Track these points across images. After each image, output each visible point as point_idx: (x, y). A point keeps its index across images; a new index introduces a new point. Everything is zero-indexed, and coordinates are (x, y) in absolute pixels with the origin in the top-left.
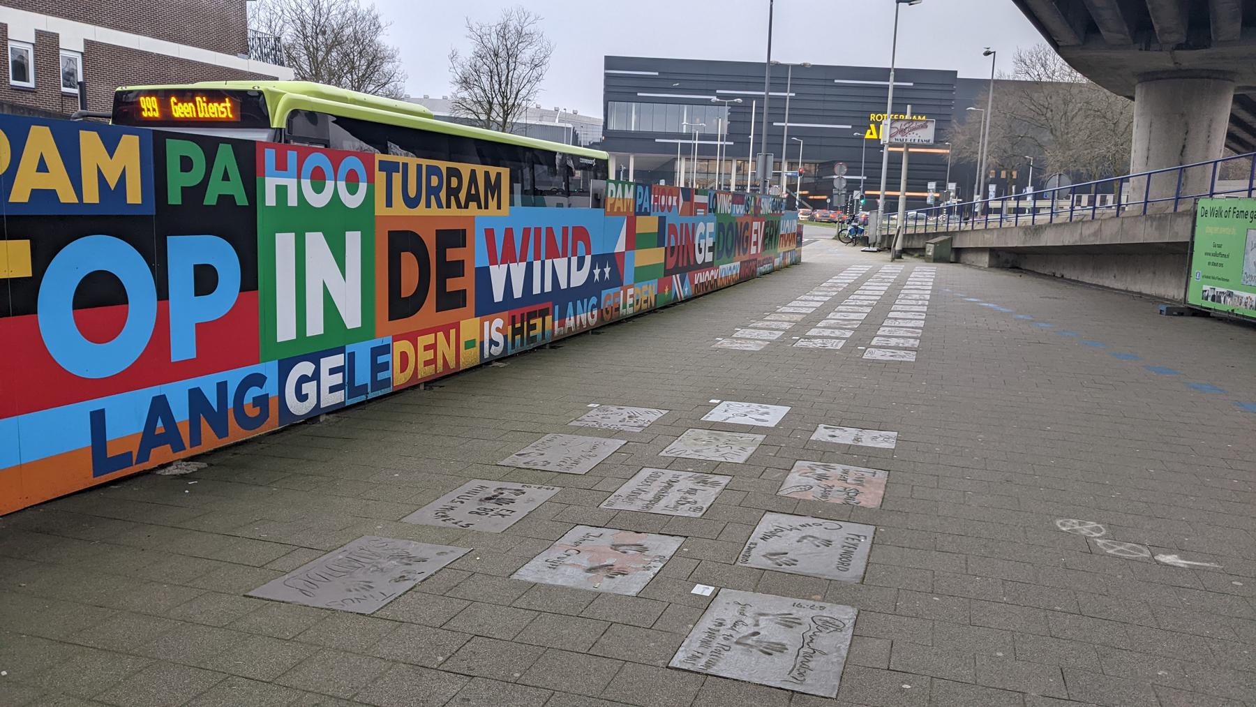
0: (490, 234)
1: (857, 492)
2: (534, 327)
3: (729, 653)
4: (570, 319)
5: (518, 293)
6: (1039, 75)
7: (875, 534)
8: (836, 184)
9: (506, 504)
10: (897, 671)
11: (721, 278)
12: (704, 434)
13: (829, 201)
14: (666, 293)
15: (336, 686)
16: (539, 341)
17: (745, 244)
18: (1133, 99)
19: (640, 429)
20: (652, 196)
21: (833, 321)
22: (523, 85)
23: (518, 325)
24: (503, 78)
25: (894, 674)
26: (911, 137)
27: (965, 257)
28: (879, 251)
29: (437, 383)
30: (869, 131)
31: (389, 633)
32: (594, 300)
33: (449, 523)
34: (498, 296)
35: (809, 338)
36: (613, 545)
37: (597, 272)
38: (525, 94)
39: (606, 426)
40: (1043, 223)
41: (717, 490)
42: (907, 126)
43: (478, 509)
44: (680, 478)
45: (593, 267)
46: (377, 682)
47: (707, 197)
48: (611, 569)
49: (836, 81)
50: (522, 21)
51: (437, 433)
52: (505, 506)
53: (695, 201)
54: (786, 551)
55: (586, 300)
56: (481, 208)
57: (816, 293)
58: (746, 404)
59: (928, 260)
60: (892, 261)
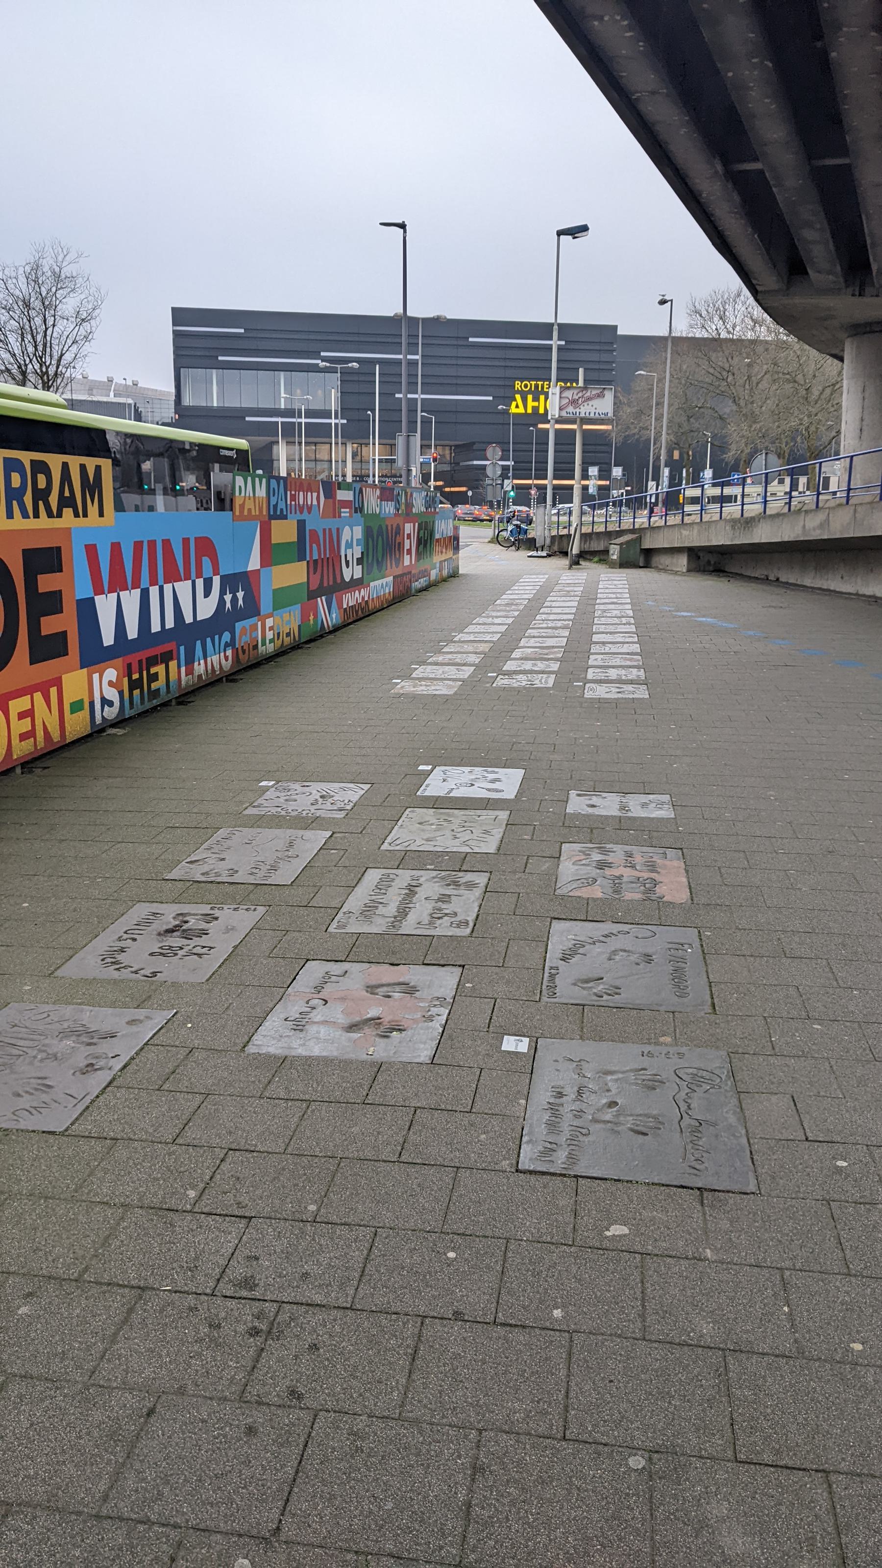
0: (91, 551)
1: (655, 883)
2: (154, 678)
3: (591, 1138)
4: (199, 664)
5: (132, 632)
6: (716, 329)
7: (701, 939)
8: (489, 472)
9: (198, 936)
10: (820, 1142)
11: (373, 599)
12: (429, 814)
13: (470, 493)
14: (312, 622)
15: (50, 1259)
16: (164, 697)
17: (397, 552)
18: (841, 359)
19: (342, 815)
20: (289, 493)
21: (529, 650)
22: (66, 347)
23: (136, 676)
24: (39, 338)
25: (818, 1146)
26: (585, 410)
27: (656, 560)
28: (549, 556)
29: (39, 764)
30: (514, 404)
31: (102, 1159)
32: (226, 637)
33: (126, 974)
34: (108, 638)
35: (510, 674)
36: (368, 987)
37: (228, 598)
38: (70, 359)
39: (296, 813)
40: (752, 514)
41: (477, 894)
42: (580, 395)
43: (161, 948)
44: (422, 880)
45: (222, 593)
46: (110, 1245)
47: (351, 493)
48: (380, 1024)
49: (471, 339)
50: (60, 258)
51: (63, 838)
52: (196, 941)
53: (338, 498)
54: (602, 976)
55: (217, 637)
56: (79, 517)
57: (494, 614)
58: (467, 769)
59: (612, 565)
60: (570, 569)
